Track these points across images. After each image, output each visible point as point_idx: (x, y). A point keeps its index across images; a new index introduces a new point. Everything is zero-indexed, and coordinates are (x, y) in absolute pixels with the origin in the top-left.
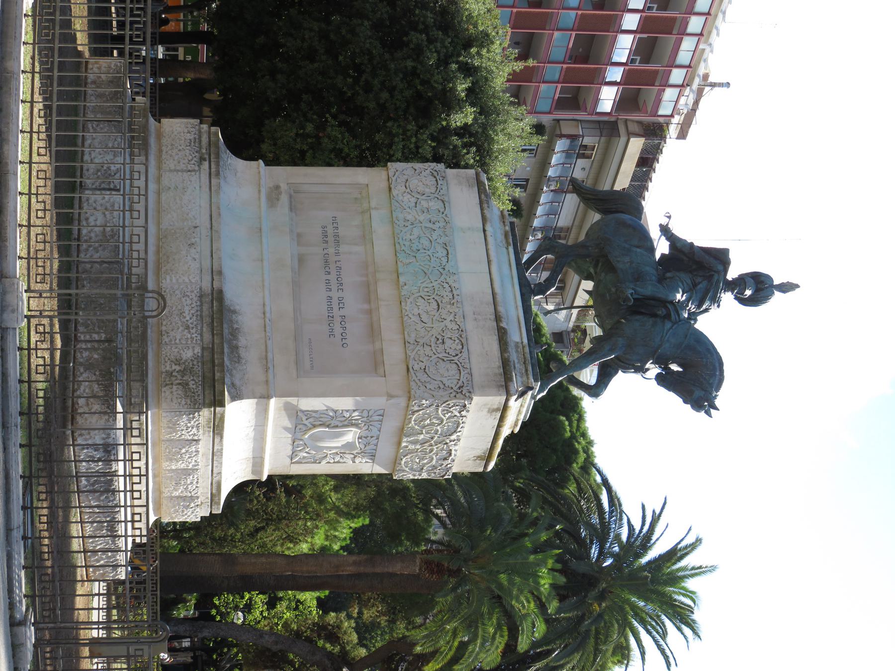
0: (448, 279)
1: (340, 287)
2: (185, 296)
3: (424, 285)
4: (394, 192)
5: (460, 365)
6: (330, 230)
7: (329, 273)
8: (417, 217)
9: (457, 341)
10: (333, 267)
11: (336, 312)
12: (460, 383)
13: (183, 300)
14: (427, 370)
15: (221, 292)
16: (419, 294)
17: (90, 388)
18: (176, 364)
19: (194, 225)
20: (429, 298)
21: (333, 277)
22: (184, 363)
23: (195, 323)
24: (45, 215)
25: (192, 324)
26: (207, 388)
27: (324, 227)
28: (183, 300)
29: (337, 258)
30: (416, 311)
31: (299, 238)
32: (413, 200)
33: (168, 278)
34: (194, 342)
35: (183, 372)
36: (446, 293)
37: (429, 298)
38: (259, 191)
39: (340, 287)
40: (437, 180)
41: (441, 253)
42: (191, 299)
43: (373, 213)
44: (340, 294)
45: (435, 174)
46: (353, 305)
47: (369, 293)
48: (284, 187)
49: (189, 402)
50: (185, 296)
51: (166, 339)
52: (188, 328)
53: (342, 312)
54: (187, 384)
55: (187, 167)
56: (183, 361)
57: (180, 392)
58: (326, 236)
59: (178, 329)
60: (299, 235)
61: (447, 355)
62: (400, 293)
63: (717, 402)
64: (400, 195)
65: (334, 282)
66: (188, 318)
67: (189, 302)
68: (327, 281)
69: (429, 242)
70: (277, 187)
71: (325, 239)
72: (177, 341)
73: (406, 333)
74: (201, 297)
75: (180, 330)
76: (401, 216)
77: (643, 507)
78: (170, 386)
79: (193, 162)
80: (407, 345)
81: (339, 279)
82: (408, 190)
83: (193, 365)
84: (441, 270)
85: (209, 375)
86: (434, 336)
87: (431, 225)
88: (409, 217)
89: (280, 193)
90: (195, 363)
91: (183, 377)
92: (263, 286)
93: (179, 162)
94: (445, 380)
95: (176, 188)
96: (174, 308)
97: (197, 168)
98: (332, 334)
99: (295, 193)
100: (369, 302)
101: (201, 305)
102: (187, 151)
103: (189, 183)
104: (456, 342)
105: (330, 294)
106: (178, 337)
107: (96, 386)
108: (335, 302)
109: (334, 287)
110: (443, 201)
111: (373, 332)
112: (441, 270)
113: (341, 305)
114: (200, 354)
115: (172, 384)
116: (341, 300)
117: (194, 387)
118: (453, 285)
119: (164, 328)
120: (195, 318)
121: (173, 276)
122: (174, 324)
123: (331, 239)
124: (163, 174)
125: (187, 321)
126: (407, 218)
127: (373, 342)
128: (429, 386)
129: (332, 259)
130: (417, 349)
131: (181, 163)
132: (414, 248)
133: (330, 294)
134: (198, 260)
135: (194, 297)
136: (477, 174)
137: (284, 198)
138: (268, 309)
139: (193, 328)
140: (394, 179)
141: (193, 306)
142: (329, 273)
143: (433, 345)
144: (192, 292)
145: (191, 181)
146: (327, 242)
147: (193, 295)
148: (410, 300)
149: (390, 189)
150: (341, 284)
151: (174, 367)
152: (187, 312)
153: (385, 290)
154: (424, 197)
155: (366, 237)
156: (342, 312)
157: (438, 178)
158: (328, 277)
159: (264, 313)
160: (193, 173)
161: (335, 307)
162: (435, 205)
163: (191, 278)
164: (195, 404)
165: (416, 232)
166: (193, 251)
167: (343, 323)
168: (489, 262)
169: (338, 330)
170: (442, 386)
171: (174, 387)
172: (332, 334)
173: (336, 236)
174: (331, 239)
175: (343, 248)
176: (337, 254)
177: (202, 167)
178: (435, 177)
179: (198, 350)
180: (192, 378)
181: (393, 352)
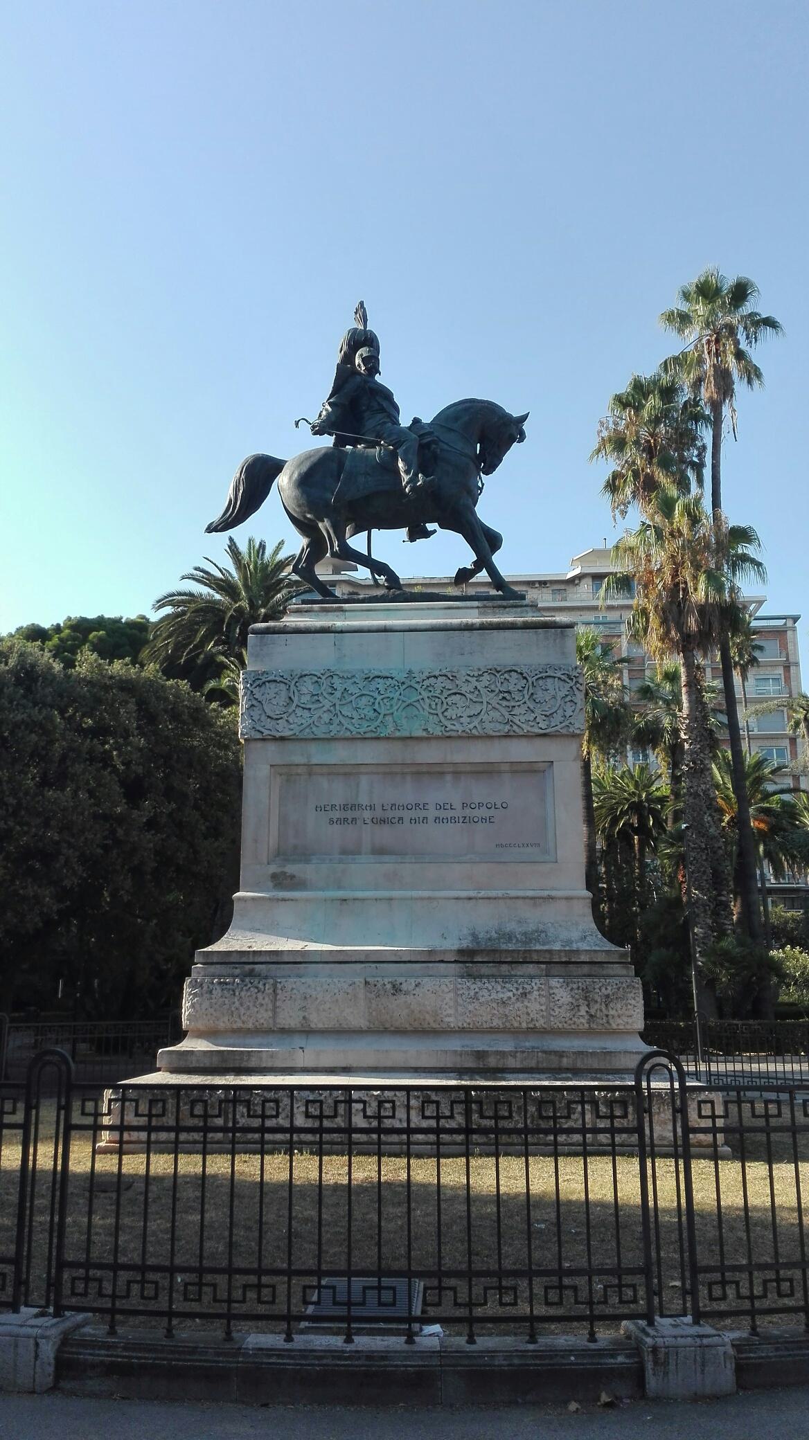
0: (417, 680)
1: (421, 806)
2: (476, 997)
3: (426, 707)
4: (287, 733)
5: (286, 681)
6: (337, 815)
7: (401, 819)
8: (325, 709)
9: (506, 675)
10: (390, 814)
11: (458, 813)
12: (563, 677)
13: (482, 1000)
14: (548, 713)
15: (461, 952)
16: (440, 715)
17: (666, 1123)
18: (579, 1010)
19: (362, 986)
20: (445, 704)
21: (407, 815)
22: (577, 1000)
23: (515, 985)
24: (732, 1282)
25: (517, 989)
26: (605, 972)
27: (331, 821)
28: (482, 1000)
29: (378, 808)
30: (465, 720)
31: (349, 852)
32: (299, 712)
33: (447, 1019)
34: (543, 987)
35: (589, 1001)
36: (440, 683)
37: (445, 704)
38: (284, 900)
39: (421, 806)
40: (269, 682)
41: (381, 684)
42: (480, 989)
43: (314, 761)
44: (431, 807)
45: (258, 682)
46: (449, 793)
47: (435, 772)
48: (273, 869)
49: (632, 995)
50: (476, 997)
51: (540, 1023)
52: (524, 995)
53: (458, 805)
54: (607, 996)
55: (268, 995)
56: (574, 1002)
57: (619, 1006)
58: (346, 820)
59: (527, 1007)
60: (344, 852)
61: (526, 688)
62: (438, 738)
63: (516, 413)
64: (292, 726)
65: (413, 814)
66: (510, 994)
67: (485, 992)
68: (437, 821)
69: (364, 697)
70: (274, 877)
71: (349, 821)
72: (543, 1008)
73: (494, 734)
74: (470, 976)
75: (529, 1005)
76: (324, 729)
77: (282, 543)
78: (610, 1017)
79: (261, 986)
80: (511, 733)
81: (410, 807)
82: (285, 716)
83: (578, 988)
84: (404, 686)
85: (586, 969)
86: (500, 702)
87: (338, 694)
88: (326, 717)
89: (284, 873)
90: (575, 986)
91: (596, 1002)
92: (429, 898)
93: (262, 1005)
94: (562, 694)
95: (304, 1008)
96: (496, 1012)
97: (271, 981)
98: (490, 820)
99: (281, 854)
100: (442, 773)
101: (488, 977)
102: (243, 994)
103: (295, 991)
104: (508, 677)
105: (431, 819)
106: (538, 1007)
107: (662, 1115)
108: (442, 814)
109: (422, 814)
110: (301, 677)
111: (487, 771)
112: (404, 686)
113: (448, 807)
114: (561, 980)
115: (607, 1016)
116: (440, 807)
117: (609, 988)
118: (426, 674)
119: (524, 1025)
120: (507, 985)
121: (445, 1013)
122: (518, 1013)
123: (349, 815)
124: (278, 1026)
125: (514, 995)
126: (328, 721)
127: (499, 772)
128: (569, 713)
129: (379, 813)
130: (518, 723)
131: (263, 1002)
132: (371, 714)
133: (431, 819)
134: (419, 980)
135: (475, 986)
136: (255, 632)
137: (290, 869)
138: (464, 894)
139: (523, 988)
140: (266, 732)
141: (490, 988)
142: (401, 819)
143: (513, 704)
144: (469, 988)
145: (292, 989)
146: (354, 820)
147: (473, 987)
148: (449, 726)
149: (282, 739)
150: (417, 805)
151: (583, 1012)
152: (501, 995)
153: (429, 754)
154: (296, 699)
155: (349, 772)
156: (458, 805)
157: (264, 680)
158: (406, 820)
159: (470, 899)
160: (279, 986)
161: (450, 814)
162: (308, 686)
163: (446, 990)
164: (634, 987)
165: (347, 711)
166: (404, 987)
167: (473, 806)
168: (385, 630)
169: (483, 813)
170: (569, 698)
171: (612, 1012)
172: (490, 820)
173: (345, 807)
174: (349, 815)
175: (364, 800)
176: (372, 808)
177: (264, 973)
178: (264, 683)
179: (554, 982)
180: (597, 991)
181: (522, 751)
